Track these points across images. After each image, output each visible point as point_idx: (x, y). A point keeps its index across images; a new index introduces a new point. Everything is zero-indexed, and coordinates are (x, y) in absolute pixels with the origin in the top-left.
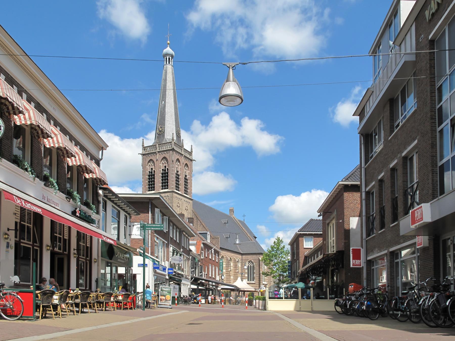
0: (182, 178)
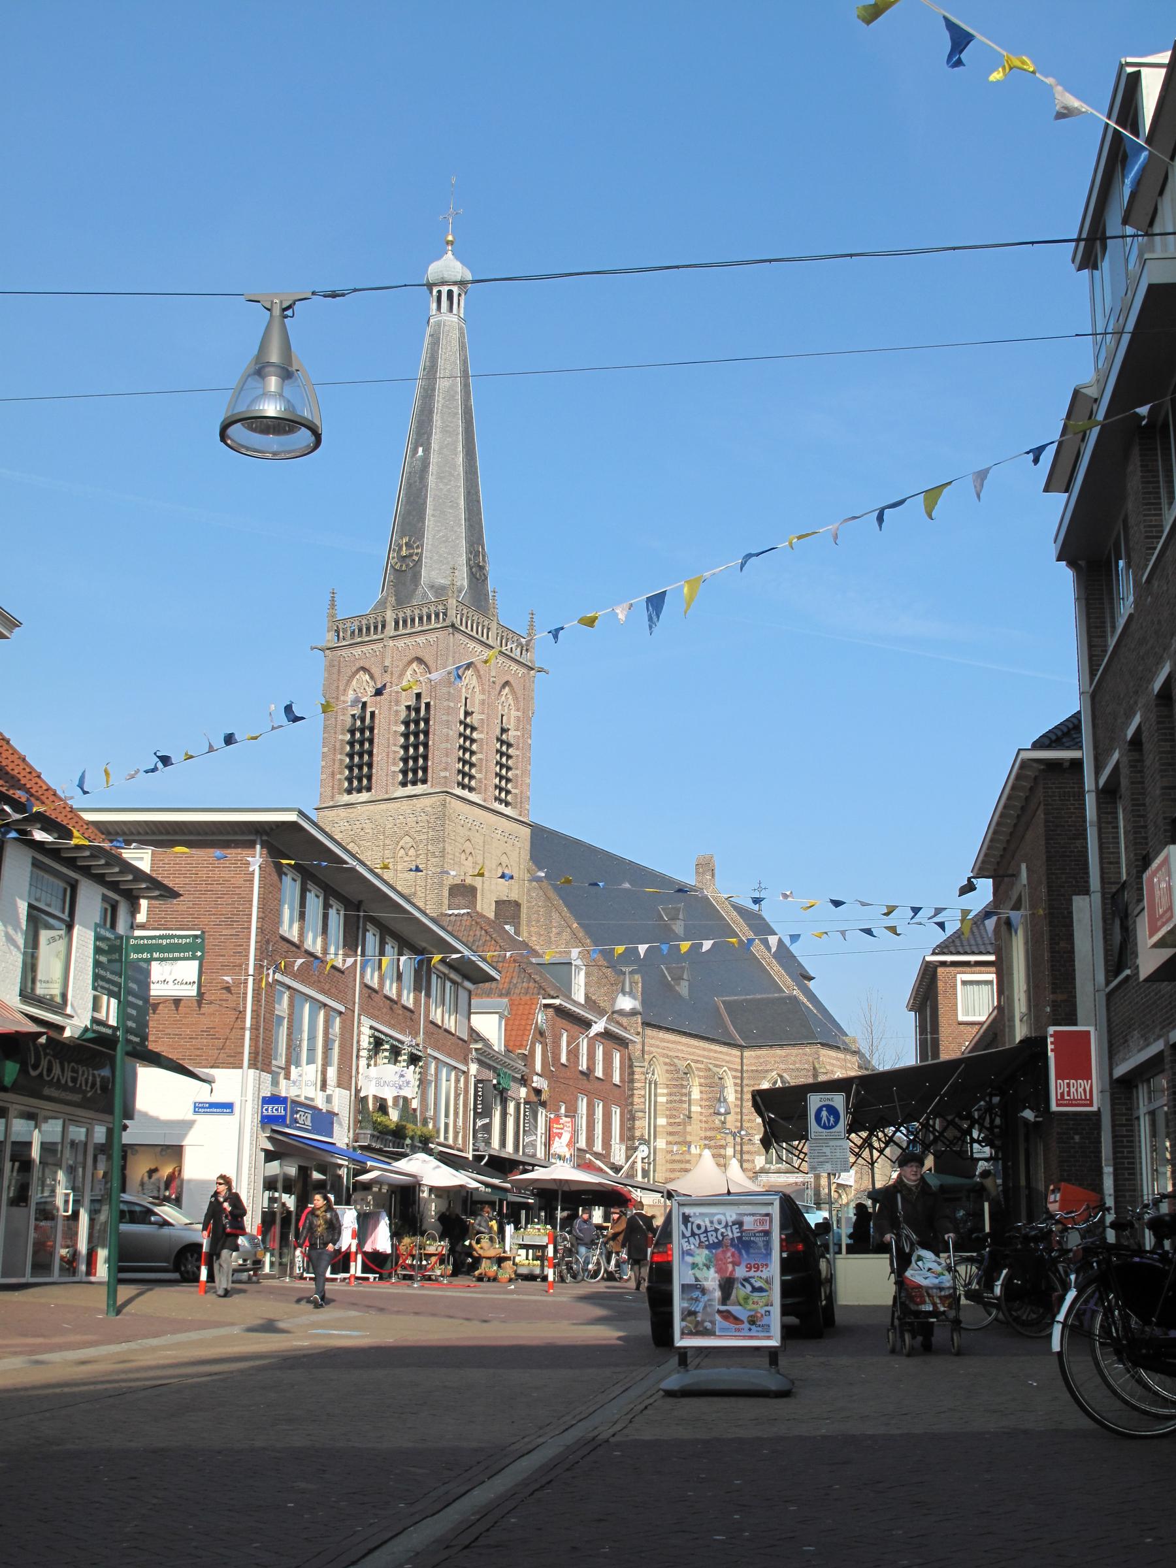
0: (485, 738)
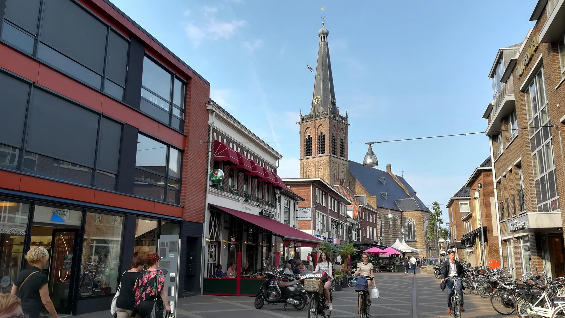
0: (338, 142)
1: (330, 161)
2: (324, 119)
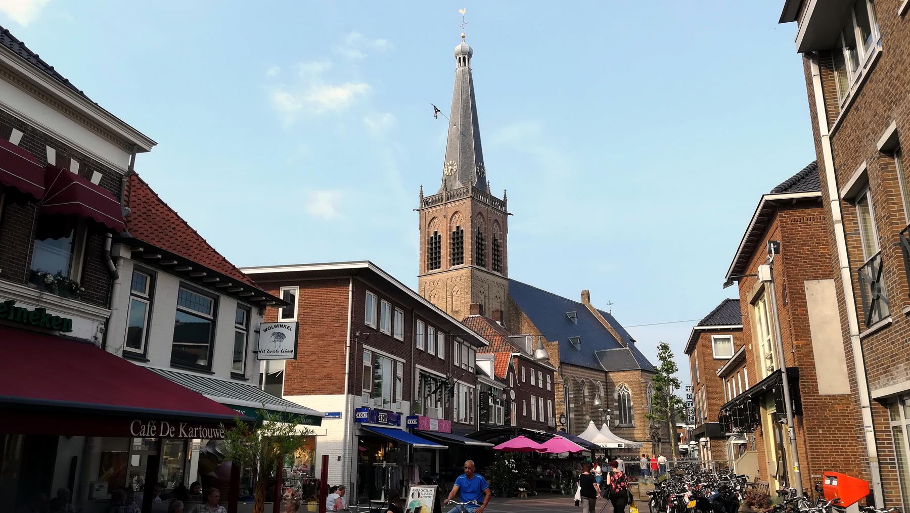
0: (488, 243)
1: (473, 277)
2: (462, 202)
